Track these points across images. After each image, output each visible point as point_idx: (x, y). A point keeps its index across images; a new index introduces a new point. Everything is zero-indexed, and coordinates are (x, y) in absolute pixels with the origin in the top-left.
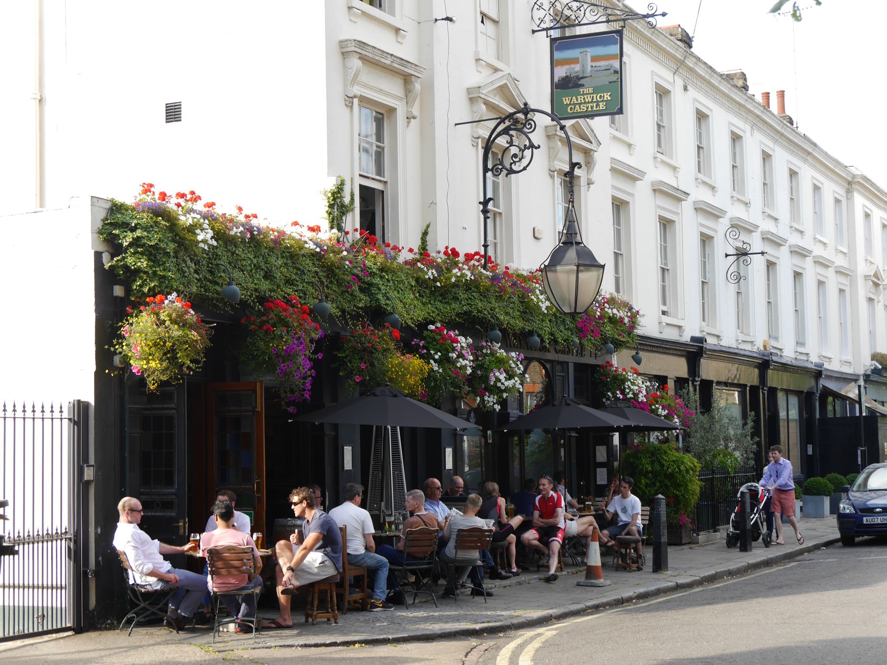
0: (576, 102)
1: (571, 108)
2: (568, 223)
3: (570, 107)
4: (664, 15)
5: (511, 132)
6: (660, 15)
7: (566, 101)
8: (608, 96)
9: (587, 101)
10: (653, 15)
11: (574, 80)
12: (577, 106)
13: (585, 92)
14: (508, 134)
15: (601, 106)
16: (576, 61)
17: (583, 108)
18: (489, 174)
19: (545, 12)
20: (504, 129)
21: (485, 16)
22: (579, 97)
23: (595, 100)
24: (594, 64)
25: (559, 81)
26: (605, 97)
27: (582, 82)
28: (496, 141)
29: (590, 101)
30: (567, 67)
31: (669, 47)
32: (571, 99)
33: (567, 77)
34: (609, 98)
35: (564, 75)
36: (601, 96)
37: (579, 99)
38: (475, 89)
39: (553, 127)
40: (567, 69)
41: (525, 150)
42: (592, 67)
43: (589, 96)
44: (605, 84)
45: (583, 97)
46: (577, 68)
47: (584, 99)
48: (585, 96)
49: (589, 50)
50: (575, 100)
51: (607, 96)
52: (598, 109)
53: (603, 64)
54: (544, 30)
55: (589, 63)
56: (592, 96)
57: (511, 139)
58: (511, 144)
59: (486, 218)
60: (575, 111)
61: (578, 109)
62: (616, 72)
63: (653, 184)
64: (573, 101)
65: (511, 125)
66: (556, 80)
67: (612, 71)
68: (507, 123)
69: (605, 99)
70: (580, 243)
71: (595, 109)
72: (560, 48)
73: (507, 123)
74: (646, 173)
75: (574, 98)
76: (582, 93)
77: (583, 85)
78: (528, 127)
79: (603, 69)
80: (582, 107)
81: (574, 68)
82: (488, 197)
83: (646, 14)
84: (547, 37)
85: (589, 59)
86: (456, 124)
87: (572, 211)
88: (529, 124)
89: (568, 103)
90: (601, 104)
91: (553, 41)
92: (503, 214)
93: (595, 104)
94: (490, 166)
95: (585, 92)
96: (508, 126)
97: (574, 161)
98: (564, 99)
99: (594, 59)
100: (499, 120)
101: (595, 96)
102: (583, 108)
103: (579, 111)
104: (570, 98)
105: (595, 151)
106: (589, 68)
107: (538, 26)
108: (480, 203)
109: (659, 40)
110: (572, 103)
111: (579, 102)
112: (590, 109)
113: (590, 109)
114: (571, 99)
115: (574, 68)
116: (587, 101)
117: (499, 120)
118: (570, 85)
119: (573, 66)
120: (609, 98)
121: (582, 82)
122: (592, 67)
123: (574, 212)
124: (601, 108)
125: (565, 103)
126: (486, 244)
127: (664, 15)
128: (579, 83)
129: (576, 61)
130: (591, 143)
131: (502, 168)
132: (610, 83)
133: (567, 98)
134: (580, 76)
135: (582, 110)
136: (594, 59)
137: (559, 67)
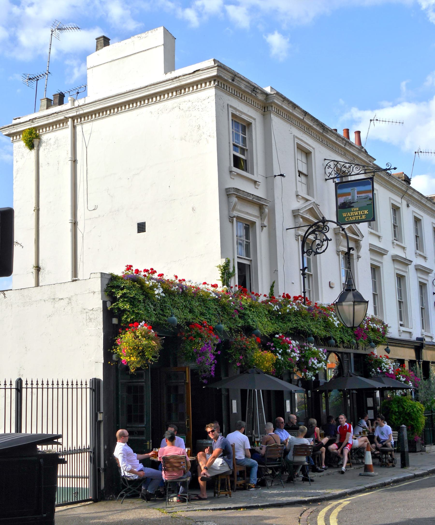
0: (350, 215)
9: (355, 215)
10: (389, 169)
12: (351, 218)
15: (363, 217)
16: (349, 194)
22: (351, 213)
23: (360, 214)
24: (359, 195)
26: (365, 212)
27: (352, 205)
30: (344, 197)
33: (344, 202)
34: (367, 213)
35: (343, 201)
37: (351, 214)
39: (338, 229)
41: (323, 241)
42: (358, 197)
45: (353, 213)
46: (350, 198)
47: (354, 213)
48: (355, 212)
49: (356, 188)
50: (349, 214)
51: (366, 212)
53: (363, 195)
54: (331, 178)
57: (316, 236)
62: (370, 199)
66: (339, 204)
67: (368, 199)
68: (314, 228)
69: (365, 213)
73: (314, 228)
75: (349, 213)
79: (364, 197)
81: (348, 198)
84: (333, 182)
85: (356, 193)
86: (287, 229)
87: (349, 273)
90: (363, 216)
91: (336, 184)
93: (360, 216)
94: (305, 250)
98: (343, 214)
101: (360, 212)
103: (351, 220)
106: (356, 198)
107: (329, 177)
111: (351, 215)
112: (357, 219)
115: (348, 198)
116: (355, 215)
118: (346, 207)
119: (347, 197)
120: (367, 213)
121: (352, 205)
122: (358, 197)
123: (351, 274)
124: (363, 218)
125: (344, 216)
130: (359, 236)
132: (367, 205)
136: (359, 193)
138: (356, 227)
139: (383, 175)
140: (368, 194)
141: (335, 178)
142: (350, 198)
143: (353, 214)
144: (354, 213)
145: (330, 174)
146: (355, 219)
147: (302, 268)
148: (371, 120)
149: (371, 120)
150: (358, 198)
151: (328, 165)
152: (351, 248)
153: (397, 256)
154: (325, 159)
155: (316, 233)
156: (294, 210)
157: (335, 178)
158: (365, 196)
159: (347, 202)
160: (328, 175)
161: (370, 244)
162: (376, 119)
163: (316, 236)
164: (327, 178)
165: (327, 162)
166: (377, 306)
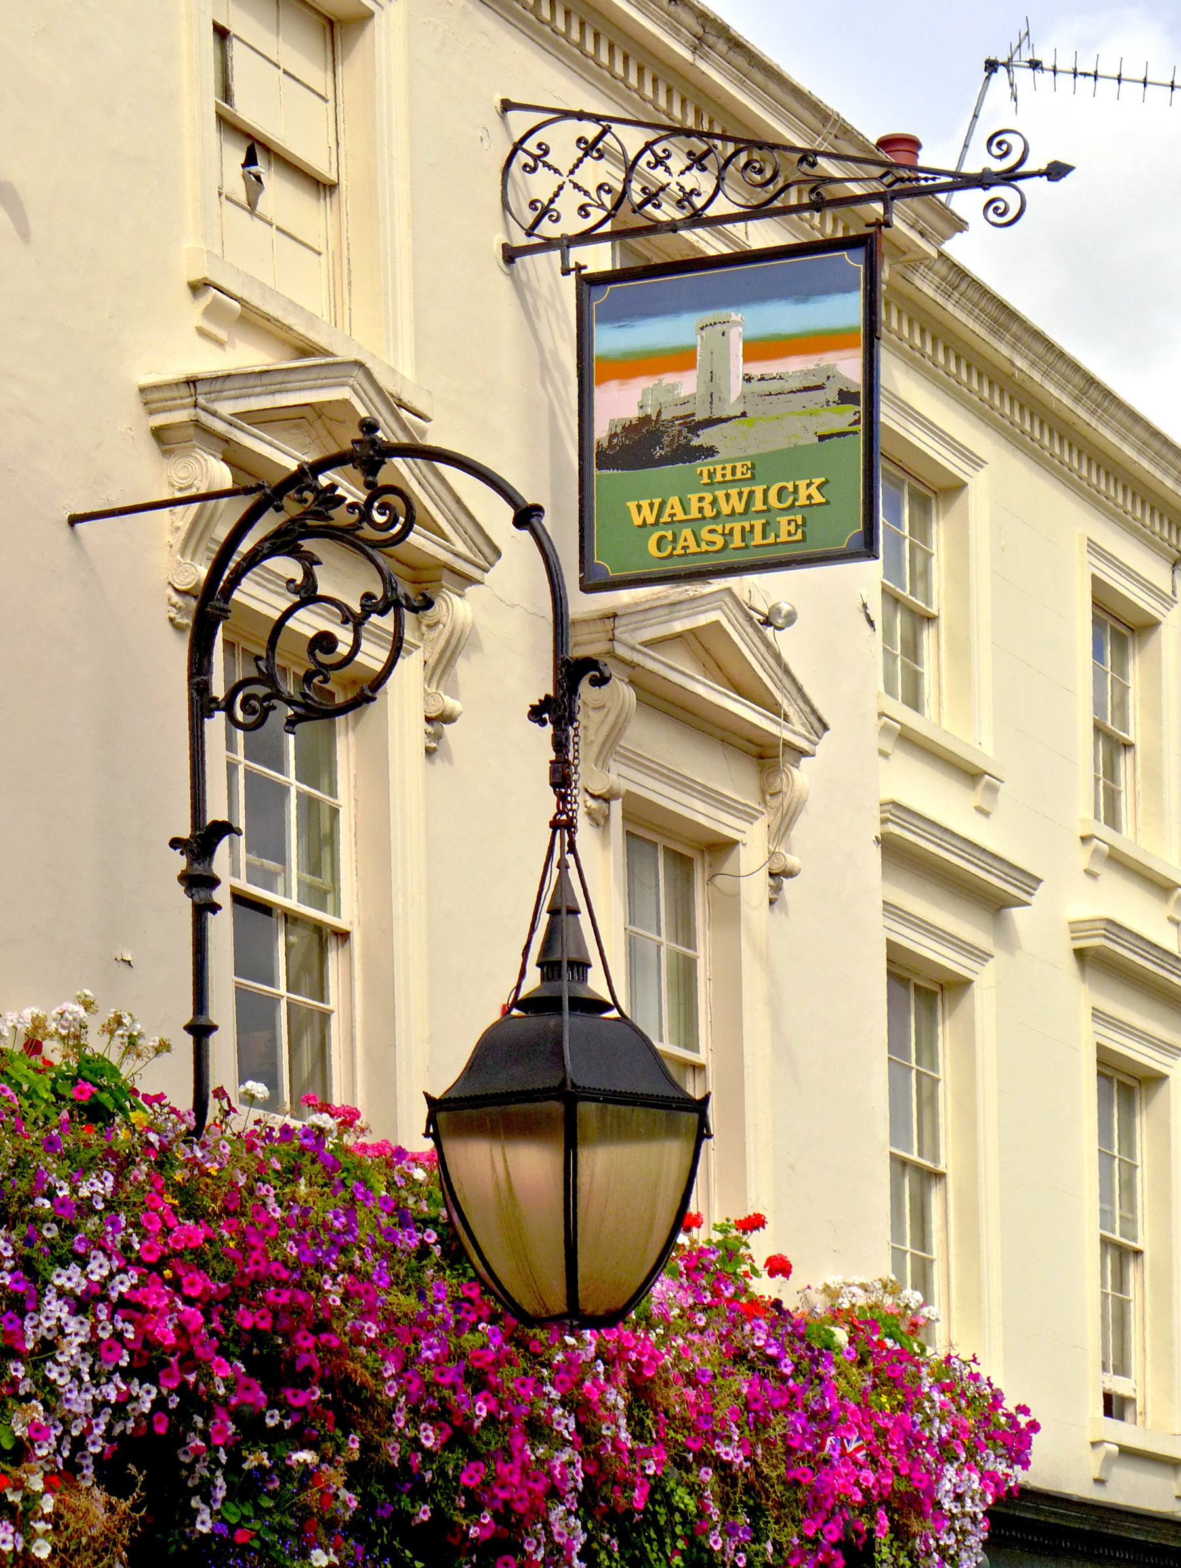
0: (680, 516)
1: (662, 538)
2: (544, 918)
3: (655, 536)
4: (1056, 171)
5: (307, 545)
6: (1039, 174)
7: (641, 512)
8: (813, 490)
9: (726, 509)
10: (1009, 177)
11: (675, 430)
12: (687, 532)
13: (719, 478)
14: (294, 552)
15: (784, 528)
16: (682, 359)
17: (712, 537)
18: (216, 725)
19: (557, 180)
20: (277, 534)
21: (267, 149)
22: (694, 498)
23: (758, 505)
24: (756, 369)
25: (612, 436)
26: (803, 493)
27: (705, 438)
28: (290, 623)
29: (740, 508)
30: (643, 384)
31: (1151, 460)
32: (662, 505)
33: (645, 420)
34: (818, 498)
35: (633, 413)
36: (781, 490)
37: (694, 506)
38: (168, 394)
39: (600, 626)
40: (644, 393)
41: (366, 614)
42: (748, 379)
43: (734, 492)
44: (802, 442)
45: (709, 497)
46: (687, 384)
47: (714, 502)
48: (720, 494)
49: (735, 315)
50: (678, 510)
51: (809, 491)
52: (771, 540)
53: (794, 366)
54: (548, 244)
55: (738, 367)
56: (746, 490)
57: (309, 575)
58: (307, 594)
59: (203, 910)
60: (679, 551)
61: (691, 542)
62: (846, 397)
63: (1077, 928)
64: (668, 511)
65: (307, 513)
66: (601, 431)
67: (832, 394)
68: (292, 507)
69: (802, 501)
70: (606, 1007)
71: (758, 539)
72: (619, 316)
73: (292, 507)
74: (1039, 881)
75: (674, 500)
76: (706, 480)
77: (710, 452)
78: (380, 519)
79: (796, 385)
80: (704, 534)
81: (674, 387)
82: (216, 811)
83: (979, 171)
84: (566, 272)
85: (737, 348)
86: (74, 520)
87: (563, 866)
88: (383, 508)
89: (651, 520)
90: (783, 520)
91: (589, 283)
92: (356, 938)
93: (758, 524)
94: (218, 690)
95: (719, 478)
96: (292, 521)
97: (576, 653)
98: (632, 505)
99: (756, 350)
100: (256, 497)
101: (759, 490)
102: (712, 537)
103: (693, 548)
104: (657, 501)
105: (803, 753)
106: (736, 387)
107: (529, 233)
108: (175, 843)
109: (1106, 424)
110: (665, 518)
111: (695, 514)
112: (737, 542)
113: (737, 542)
114: (662, 505)
115: (674, 387)
116: (726, 509)
117: (256, 497)
118: (658, 452)
119: (669, 379)
120: (818, 498)
121: (705, 438)
122: (748, 379)
123: (573, 873)
124: (784, 537)
125: (638, 521)
126: (202, 1021)
127: (1056, 171)
128: (695, 442)
129: (682, 359)
130: (786, 718)
131: (268, 697)
132: (822, 438)
133: (645, 503)
134: (699, 417)
135: (704, 547)
136: (756, 350)
137: (613, 385)
138: (768, 645)
139: (1033, 364)
140: (828, 359)
141: (586, 237)
142: (687, 384)
143: (706, 505)
144: (714, 502)
145: (546, 211)
146: (720, 541)
147: (185, 832)
148: (991, 66)
149: (991, 66)
150: (755, 386)
151: (531, 145)
152: (588, 664)
153: (1113, 927)
154: (507, 106)
155: (307, 545)
156: (157, 387)
157: (586, 237)
158: (805, 374)
159: (666, 416)
160: (530, 217)
161: (895, 809)
162: (1027, 56)
163: (309, 575)
164: (521, 240)
165: (521, 122)
166: (345, 798)
